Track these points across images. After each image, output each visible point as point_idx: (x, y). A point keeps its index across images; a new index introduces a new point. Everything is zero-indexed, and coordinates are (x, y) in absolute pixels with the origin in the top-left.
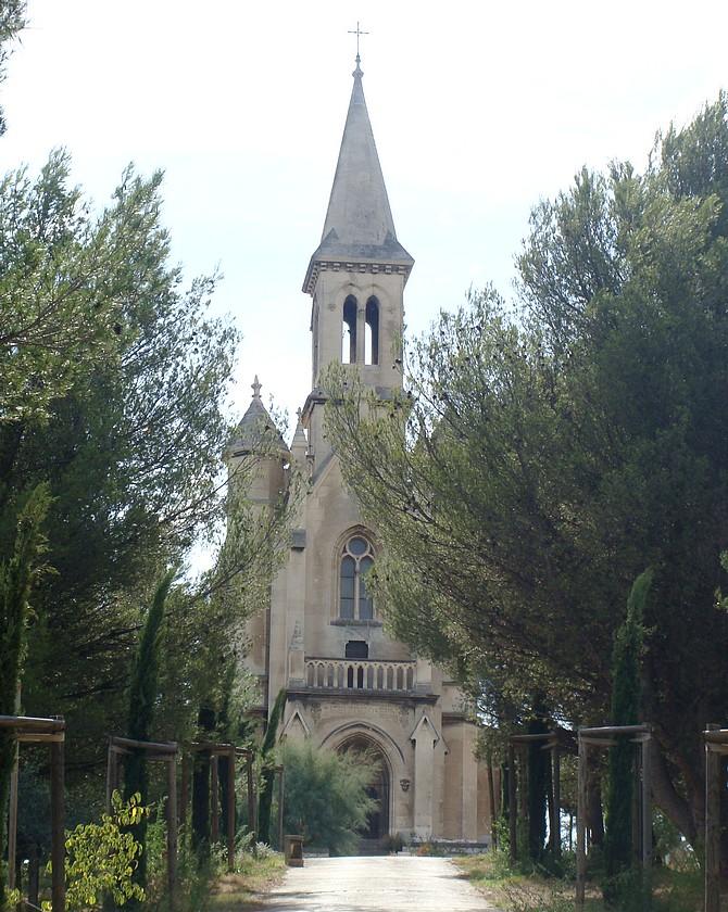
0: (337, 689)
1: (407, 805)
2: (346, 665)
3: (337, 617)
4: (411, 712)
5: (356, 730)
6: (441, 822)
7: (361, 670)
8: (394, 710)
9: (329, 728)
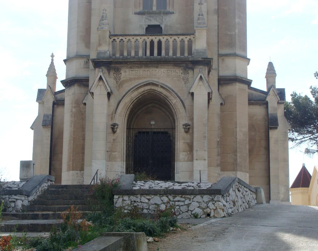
0: (134, 58)
1: (188, 144)
2: (148, 39)
3: (140, 9)
4: (190, 72)
5: (148, 87)
6: (218, 155)
7: (160, 42)
8: (178, 72)
9: (127, 87)
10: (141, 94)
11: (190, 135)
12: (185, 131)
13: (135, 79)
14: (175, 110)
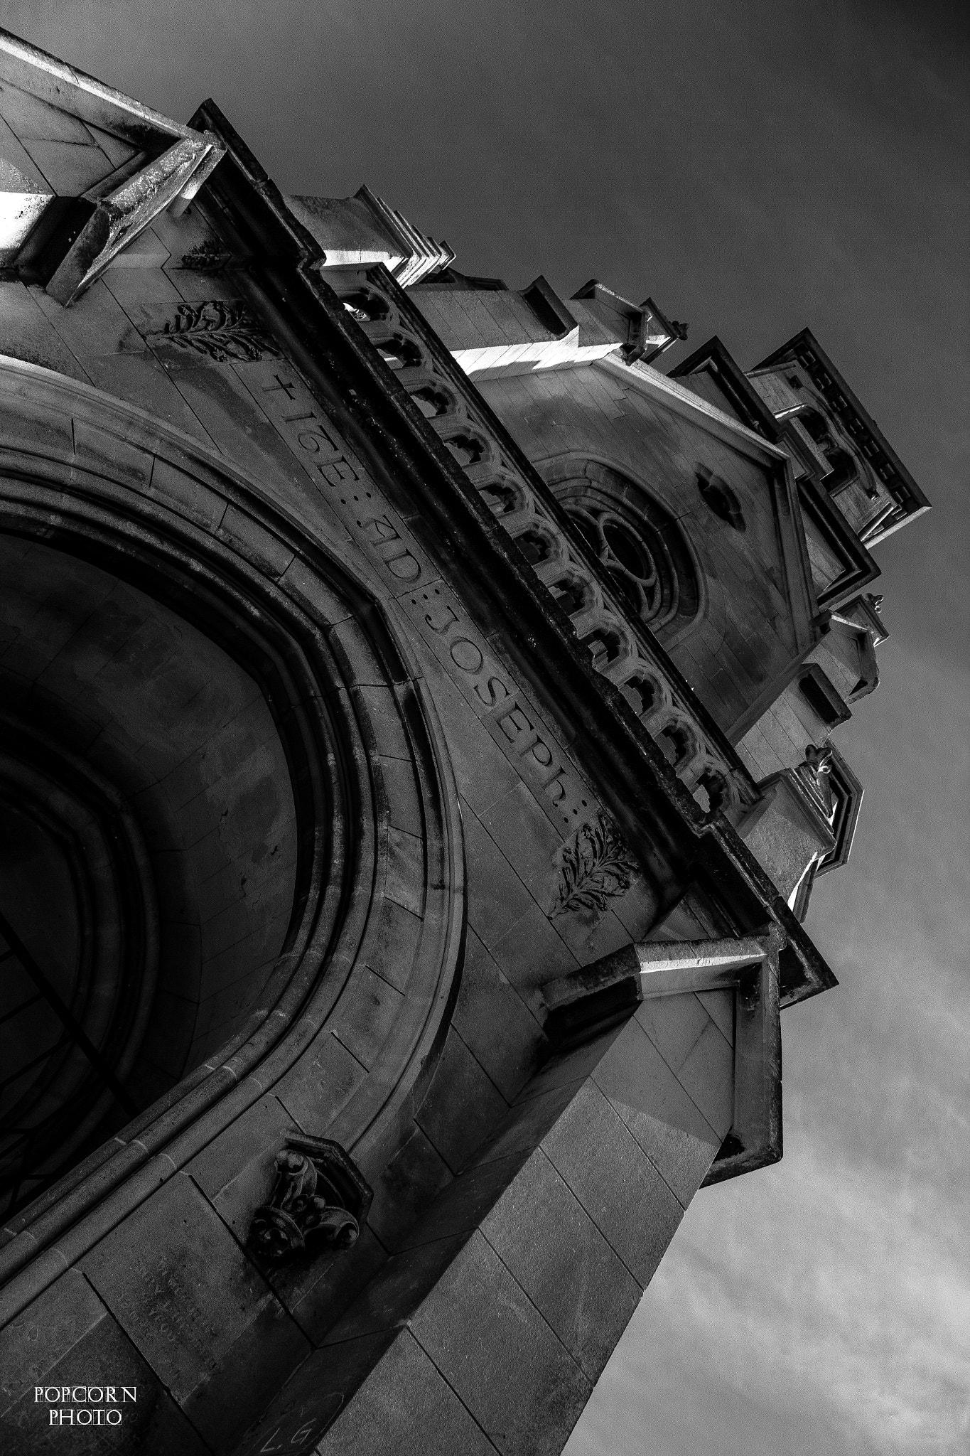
10: (225, 553)
11: (267, 1320)
12: (262, 1218)
13: (301, 472)
14: (343, 957)
